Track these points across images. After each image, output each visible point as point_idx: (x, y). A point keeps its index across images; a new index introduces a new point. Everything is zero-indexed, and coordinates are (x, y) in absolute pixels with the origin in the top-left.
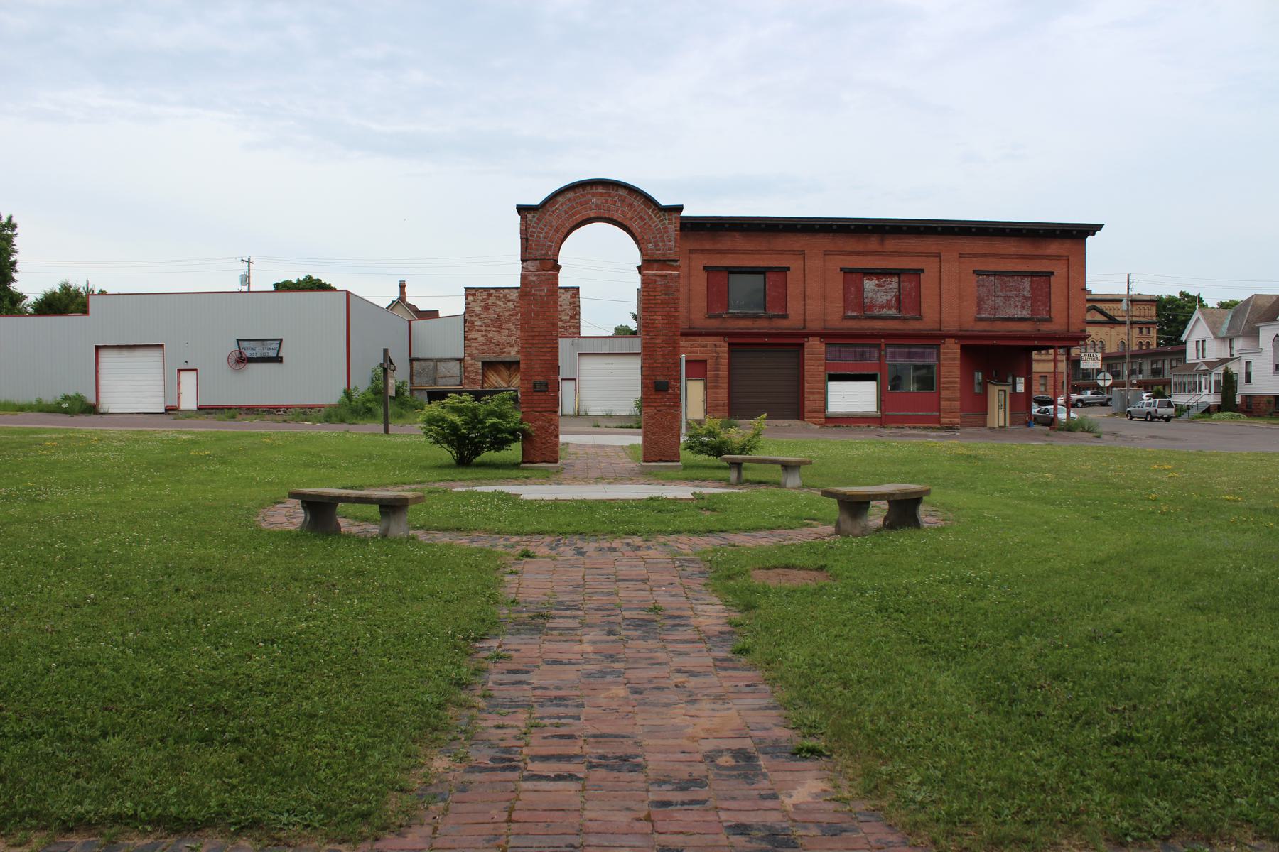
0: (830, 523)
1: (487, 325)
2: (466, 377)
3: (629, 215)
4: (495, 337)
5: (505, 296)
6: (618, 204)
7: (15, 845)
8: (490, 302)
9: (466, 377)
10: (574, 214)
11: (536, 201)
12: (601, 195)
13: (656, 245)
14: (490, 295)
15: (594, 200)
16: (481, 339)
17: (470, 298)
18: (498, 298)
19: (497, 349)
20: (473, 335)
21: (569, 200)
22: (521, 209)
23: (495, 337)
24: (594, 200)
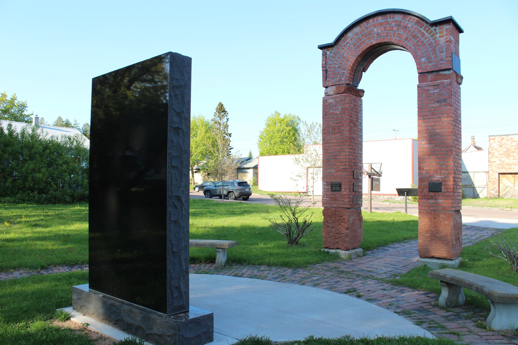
0: (83, 263)
1: (501, 155)
2: (490, 181)
3: (404, 36)
4: (506, 160)
5: (511, 139)
6: (395, 29)
7: (396, 313)
8: (503, 142)
9: (490, 181)
10: (361, 44)
11: (331, 40)
12: (381, 24)
13: (429, 58)
14: (503, 139)
15: (375, 30)
16: (498, 162)
17: (492, 141)
18: (507, 140)
19: (507, 167)
20: (493, 159)
21: (357, 34)
22: (321, 48)
23: (506, 160)
24: (375, 30)
